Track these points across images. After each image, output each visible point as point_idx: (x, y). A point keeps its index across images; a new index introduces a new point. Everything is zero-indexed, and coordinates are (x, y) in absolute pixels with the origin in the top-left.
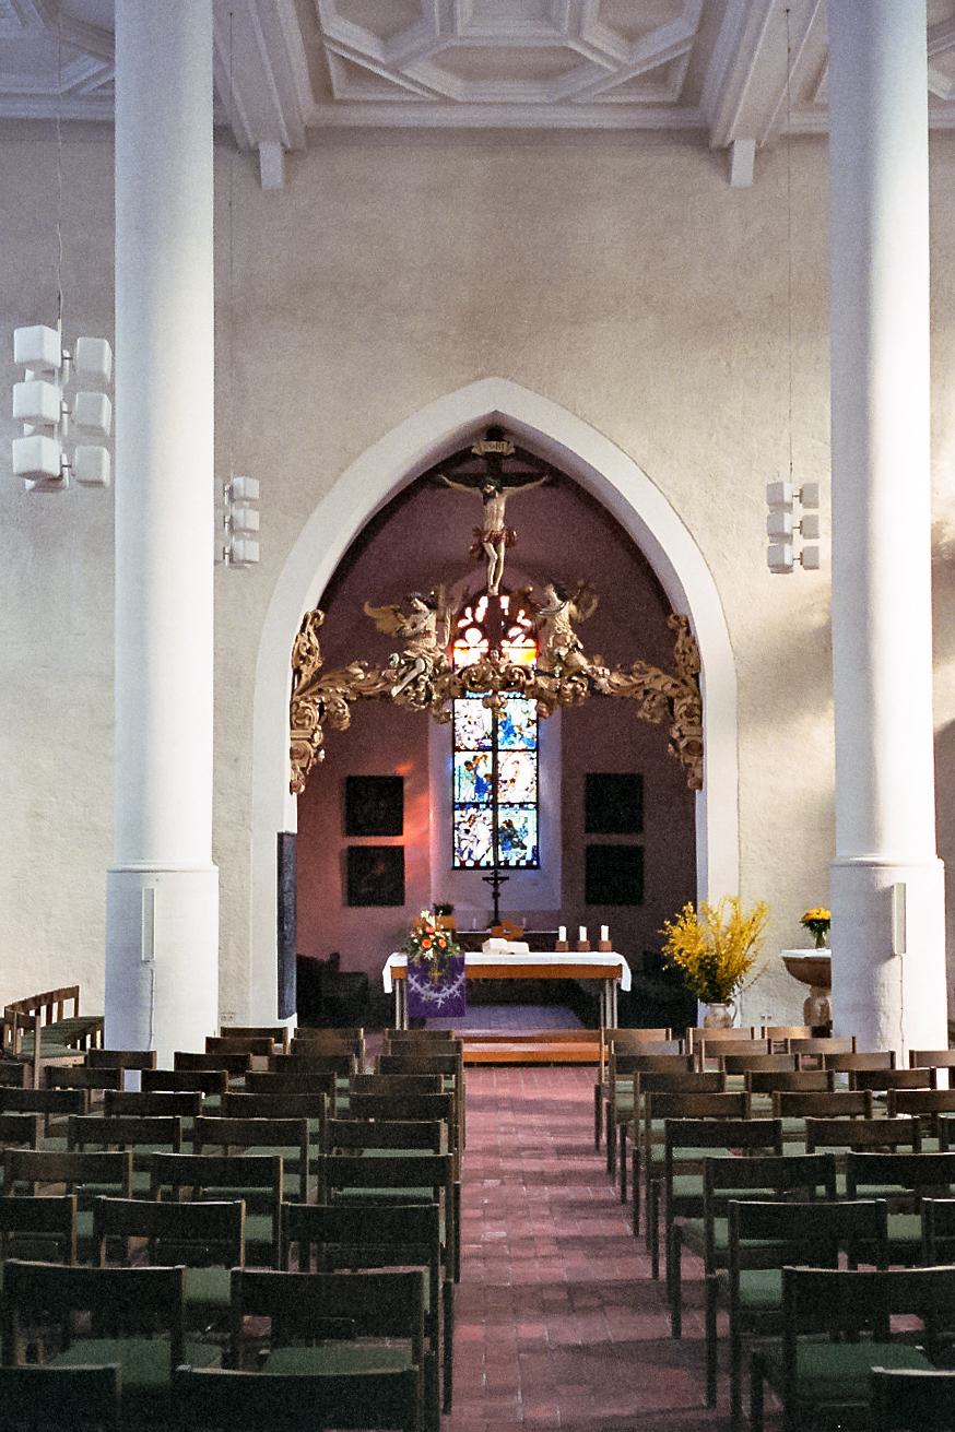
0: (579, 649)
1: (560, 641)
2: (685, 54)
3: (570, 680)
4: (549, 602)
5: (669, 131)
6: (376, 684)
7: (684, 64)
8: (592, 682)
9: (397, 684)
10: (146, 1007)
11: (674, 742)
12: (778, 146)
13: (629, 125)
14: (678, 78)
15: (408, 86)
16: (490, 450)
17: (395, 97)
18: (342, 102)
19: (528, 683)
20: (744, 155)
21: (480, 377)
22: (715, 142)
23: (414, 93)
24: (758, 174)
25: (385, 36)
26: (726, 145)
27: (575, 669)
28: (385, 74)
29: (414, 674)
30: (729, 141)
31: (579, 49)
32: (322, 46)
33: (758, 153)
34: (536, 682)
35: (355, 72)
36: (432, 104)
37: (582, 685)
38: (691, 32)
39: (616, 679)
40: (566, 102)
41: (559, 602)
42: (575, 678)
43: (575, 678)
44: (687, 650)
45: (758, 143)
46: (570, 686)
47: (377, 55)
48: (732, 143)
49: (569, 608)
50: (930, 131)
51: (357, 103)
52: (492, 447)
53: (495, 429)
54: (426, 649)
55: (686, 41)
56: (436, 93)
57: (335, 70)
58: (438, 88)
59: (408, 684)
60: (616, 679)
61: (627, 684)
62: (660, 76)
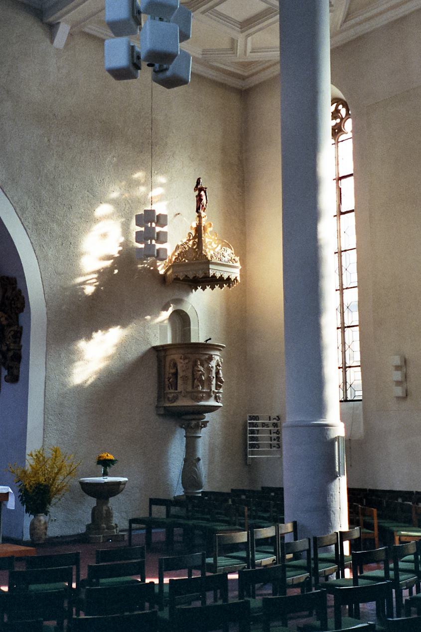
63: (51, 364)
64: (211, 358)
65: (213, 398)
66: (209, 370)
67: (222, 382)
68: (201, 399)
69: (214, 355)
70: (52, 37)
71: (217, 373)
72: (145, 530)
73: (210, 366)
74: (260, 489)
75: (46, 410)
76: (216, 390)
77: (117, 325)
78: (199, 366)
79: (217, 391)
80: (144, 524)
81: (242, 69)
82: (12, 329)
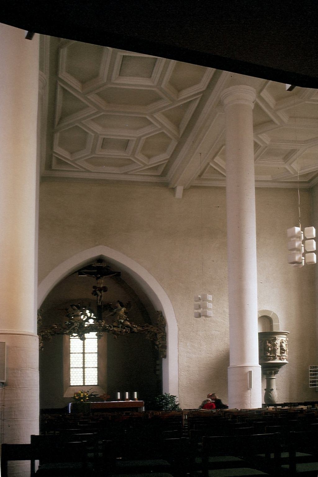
0: (127, 320)
1: (121, 318)
2: (165, 163)
3: (124, 329)
4: (117, 307)
5: (156, 183)
6: (61, 330)
7: (164, 165)
8: (131, 329)
9: (68, 330)
10: (249, 403)
11: (157, 345)
12: (190, 188)
13: (149, 181)
14: (161, 170)
15: (75, 166)
16: (98, 265)
17: (75, 170)
18: (54, 170)
19: (111, 329)
20: (179, 190)
21: (97, 245)
22: (171, 186)
23: (78, 169)
24: (183, 195)
25: (72, 153)
26: (174, 187)
27: (126, 326)
28: (70, 163)
29: (73, 327)
30: (175, 186)
31: (133, 159)
32: (52, 154)
33: (184, 189)
34: (113, 329)
35: (60, 162)
36: (83, 172)
37: (128, 330)
38: (168, 157)
39: (139, 328)
40: (126, 173)
41: (120, 307)
42: (126, 328)
43: (126, 328)
44: (161, 320)
45: (184, 187)
46: (125, 330)
47: (69, 158)
48: (176, 187)
49: (123, 309)
50: (255, 188)
51: (59, 170)
52: (99, 265)
53: (100, 259)
54: (78, 320)
55: (166, 159)
56: (85, 169)
57: (54, 161)
58: (86, 168)
59: (71, 330)
60: (139, 328)
61: (142, 329)
62: (156, 168)
63: (181, 348)
64: (275, 339)
65: (278, 358)
66: (274, 345)
67: (284, 350)
68: (269, 360)
69: (278, 337)
70: (174, 195)
71: (281, 346)
72: (292, 240)
73: (275, 343)
74: (28, 441)
75: (180, 370)
76: (281, 354)
77: (230, 412)
78: (268, 344)
79: (281, 355)
80: (71, 412)
81: (234, 415)
82: (160, 334)
